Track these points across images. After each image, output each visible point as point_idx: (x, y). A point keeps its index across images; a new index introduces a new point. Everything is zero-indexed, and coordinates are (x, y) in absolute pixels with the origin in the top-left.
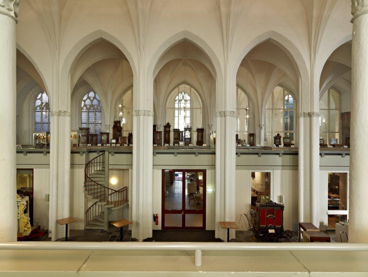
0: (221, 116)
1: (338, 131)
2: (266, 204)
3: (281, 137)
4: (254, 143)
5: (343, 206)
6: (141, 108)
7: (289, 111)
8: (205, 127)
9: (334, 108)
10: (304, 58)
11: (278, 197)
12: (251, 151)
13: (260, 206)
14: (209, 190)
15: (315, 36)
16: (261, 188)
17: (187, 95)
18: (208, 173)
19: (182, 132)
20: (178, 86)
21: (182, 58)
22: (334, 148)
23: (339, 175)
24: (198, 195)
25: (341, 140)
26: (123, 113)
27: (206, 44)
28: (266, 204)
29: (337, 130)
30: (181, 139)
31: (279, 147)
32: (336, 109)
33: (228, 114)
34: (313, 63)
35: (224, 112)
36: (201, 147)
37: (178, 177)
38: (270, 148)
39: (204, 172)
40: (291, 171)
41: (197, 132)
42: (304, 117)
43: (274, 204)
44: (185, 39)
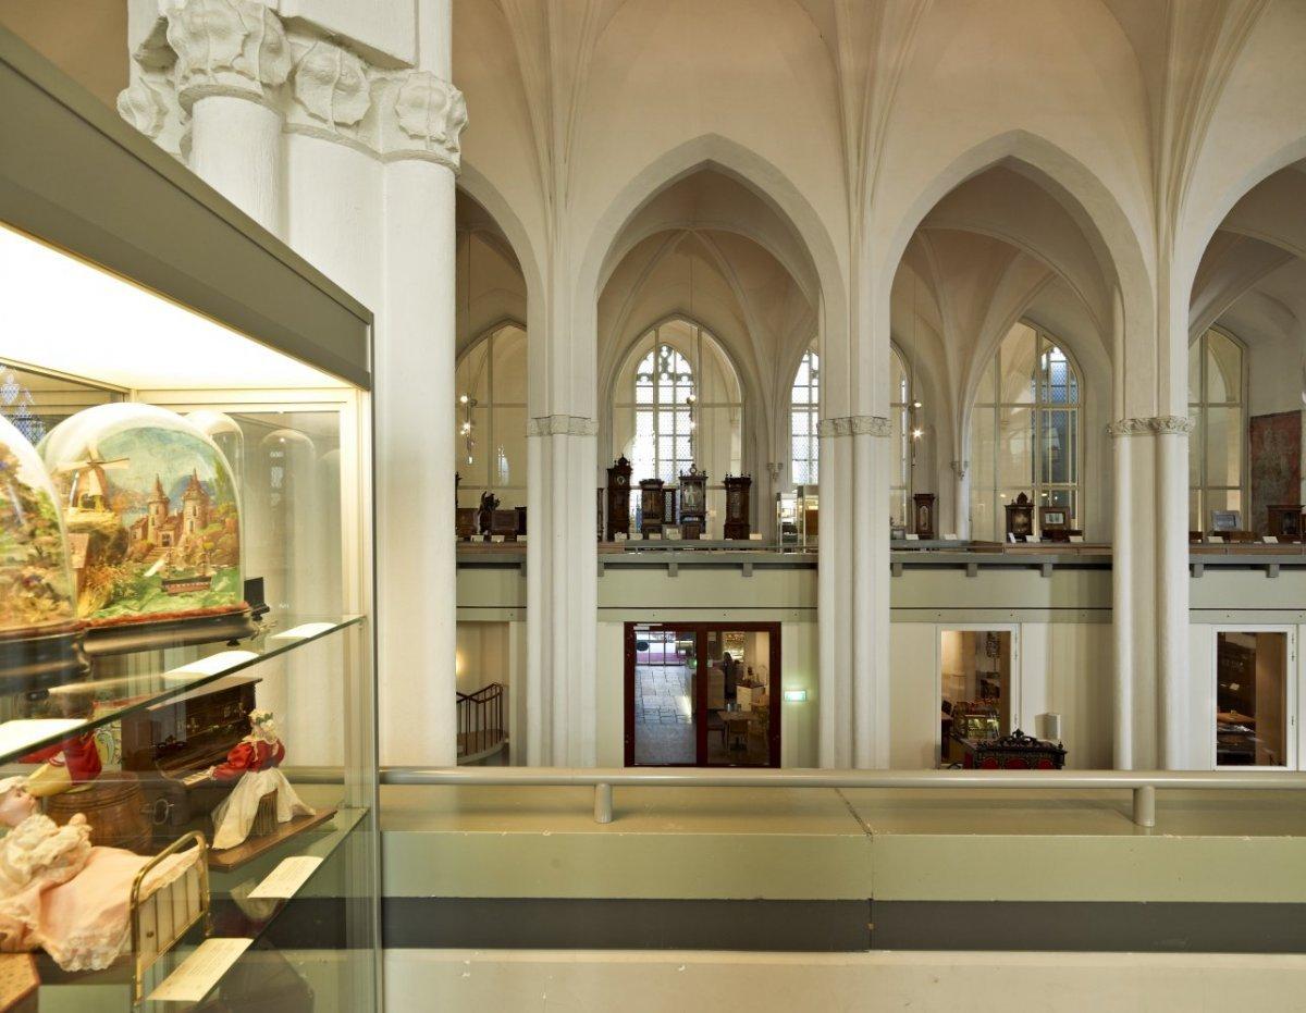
0: (838, 435)
1: (1237, 484)
2: (1002, 743)
3: (1032, 506)
4: (934, 531)
5: (1268, 751)
6: (559, 409)
7: (1050, 410)
8: (756, 472)
9: (1224, 401)
10: (1134, 227)
11: (1037, 717)
12: (923, 556)
13: (979, 751)
14: (794, 694)
15: (1174, 144)
16: (960, 691)
17: (679, 356)
18: (789, 635)
19: (673, 491)
20: (655, 325)
21: (682, 228)
22: (1228, 547)
23: (1251, 644)
24: (734, 716)
25: (1250, 516)
26: (473, 423)
27: (784, 182)
28: (1002, 743)
29: (1234, 478)
30: (668, 517)
31: (1069, 541)
32: (1229, 404)
33: (863, 426)
34: (1167, 246)
35: (851, 421)
36: (743, 543)
37: (647, 651)
38: (995, 547)
39: (774, 630)
40: (1083, 627)
41: (725, 491)
42: (1133, 435)
43: (1028, 742)
44: (709, 162)
